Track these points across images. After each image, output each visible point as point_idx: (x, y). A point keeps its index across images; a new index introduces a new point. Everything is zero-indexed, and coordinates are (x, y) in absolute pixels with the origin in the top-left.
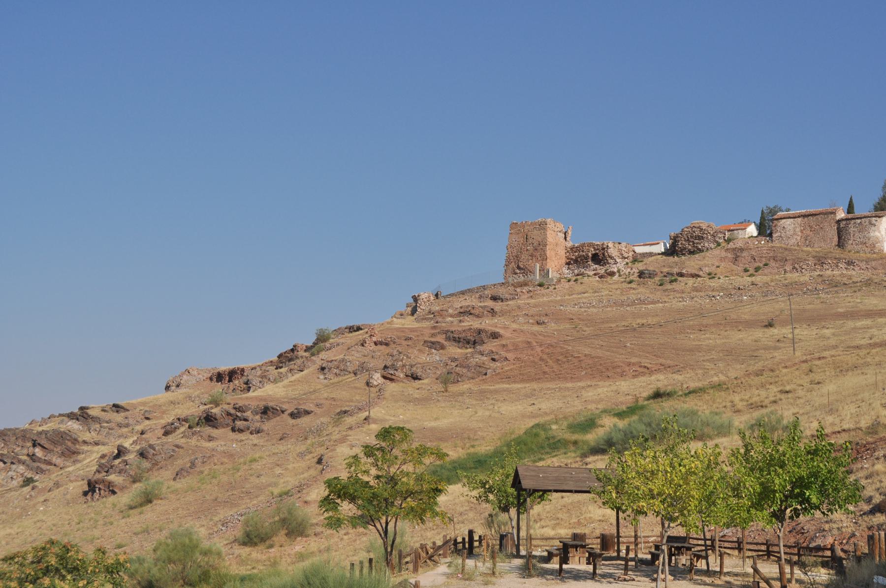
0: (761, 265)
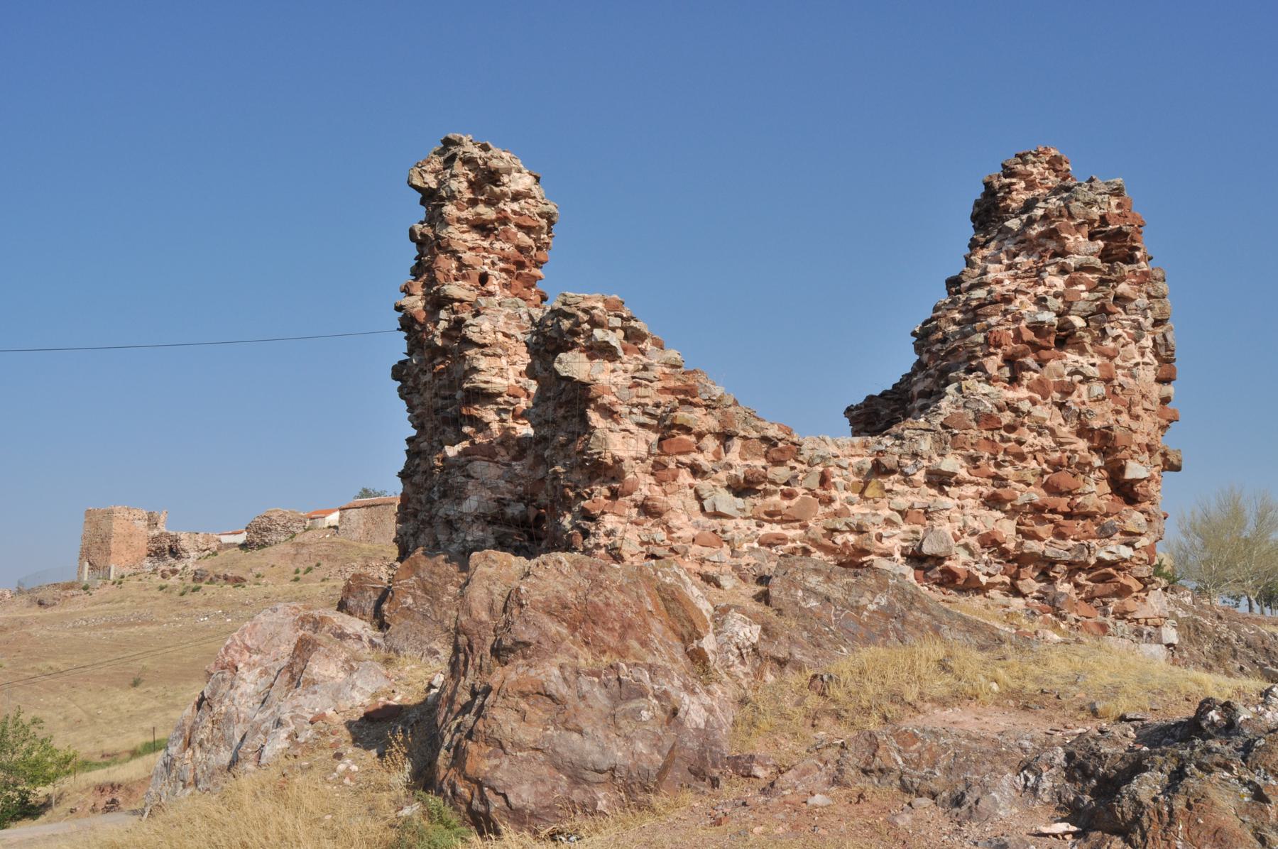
0: (313, 564)
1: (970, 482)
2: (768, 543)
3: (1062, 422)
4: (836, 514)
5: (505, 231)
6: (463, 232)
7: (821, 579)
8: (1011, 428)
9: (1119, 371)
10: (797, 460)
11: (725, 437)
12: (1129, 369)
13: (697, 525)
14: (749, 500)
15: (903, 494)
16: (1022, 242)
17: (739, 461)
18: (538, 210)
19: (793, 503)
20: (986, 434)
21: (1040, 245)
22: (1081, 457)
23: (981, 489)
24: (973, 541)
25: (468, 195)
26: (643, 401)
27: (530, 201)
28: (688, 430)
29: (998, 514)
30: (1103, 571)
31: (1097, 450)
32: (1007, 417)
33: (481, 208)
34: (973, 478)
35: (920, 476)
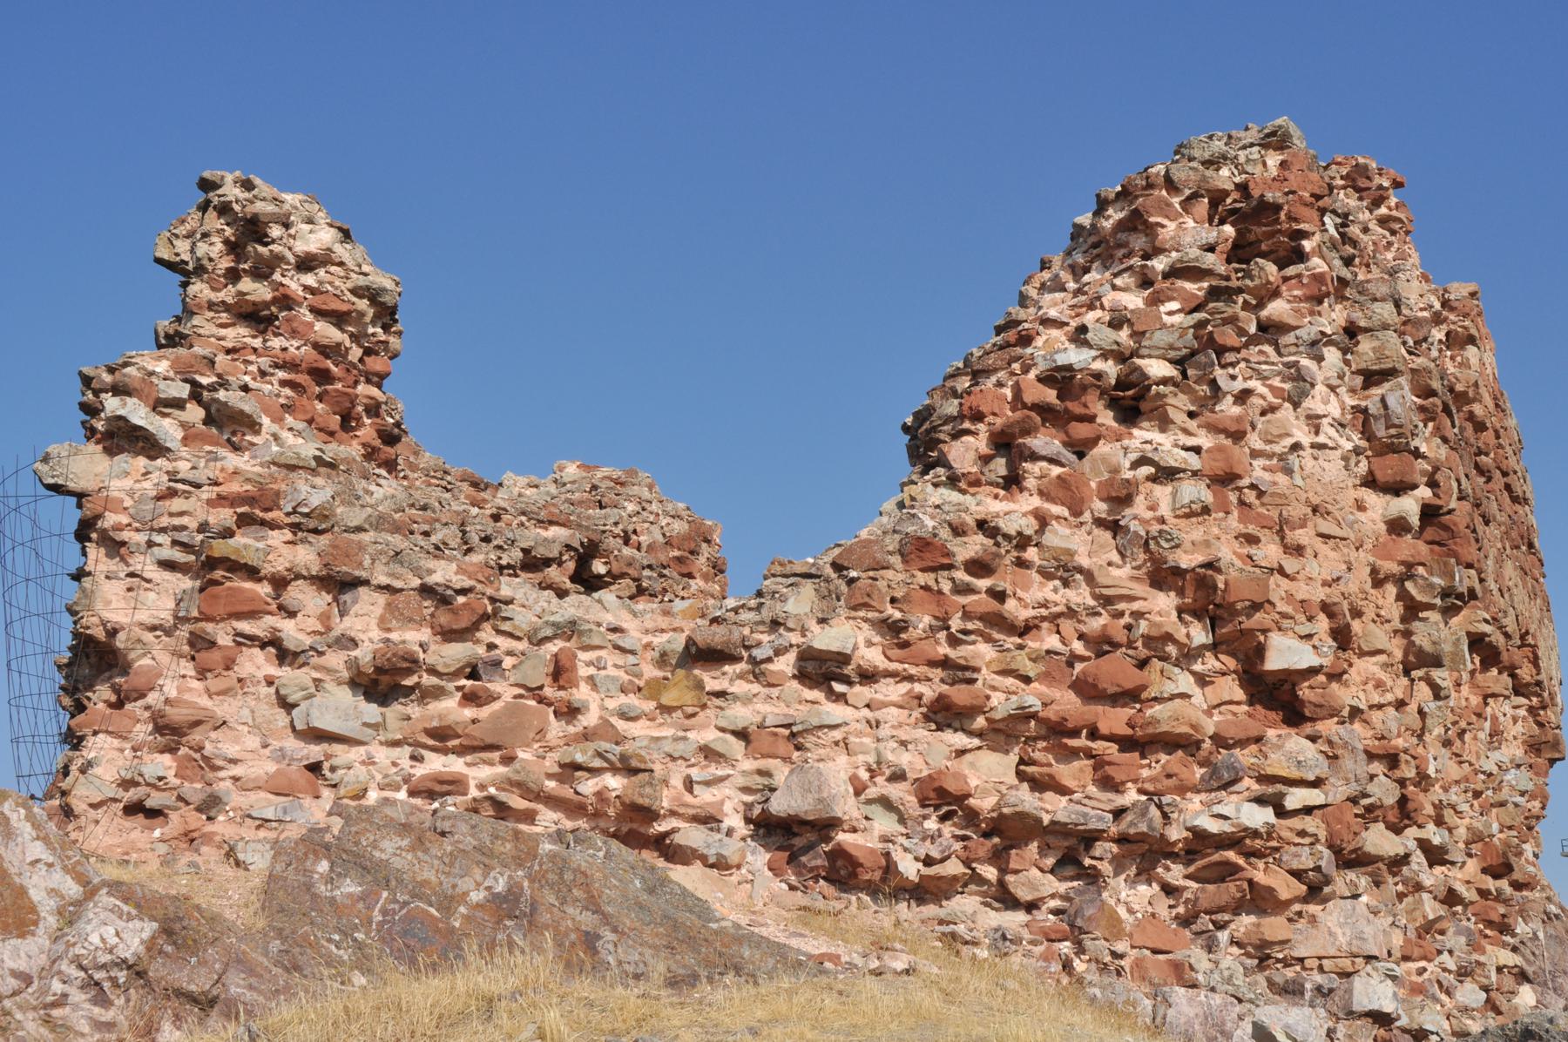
2: (431, 790)
3: (1116, 558)
4: (586, 736)
5: (288, 320)
7: (405, 843)
8: (979, 567)
9: (1258, 463)
10: (499, 632)
11: (339, 585)
12: (1282, 457)
13: (281, 755)
14: (396, 709)
15: (747, 700)
16: (1095, 246)
17: (367, 625)
18: (350, 285)
19: (484, 712)
20: (923, 578)
21: (1120, 246)
22: (1152, 624)
23: (918, 688)
24: (897, 792)
25: (226, 263)
26: (177, 521)
27: (333, 269)
28: (252, 573)
29: (960, 740)
30: (1216, 857)
31: (1198, 614)
32: (975, 545)
33: (246, 284)
35: (785, 665)
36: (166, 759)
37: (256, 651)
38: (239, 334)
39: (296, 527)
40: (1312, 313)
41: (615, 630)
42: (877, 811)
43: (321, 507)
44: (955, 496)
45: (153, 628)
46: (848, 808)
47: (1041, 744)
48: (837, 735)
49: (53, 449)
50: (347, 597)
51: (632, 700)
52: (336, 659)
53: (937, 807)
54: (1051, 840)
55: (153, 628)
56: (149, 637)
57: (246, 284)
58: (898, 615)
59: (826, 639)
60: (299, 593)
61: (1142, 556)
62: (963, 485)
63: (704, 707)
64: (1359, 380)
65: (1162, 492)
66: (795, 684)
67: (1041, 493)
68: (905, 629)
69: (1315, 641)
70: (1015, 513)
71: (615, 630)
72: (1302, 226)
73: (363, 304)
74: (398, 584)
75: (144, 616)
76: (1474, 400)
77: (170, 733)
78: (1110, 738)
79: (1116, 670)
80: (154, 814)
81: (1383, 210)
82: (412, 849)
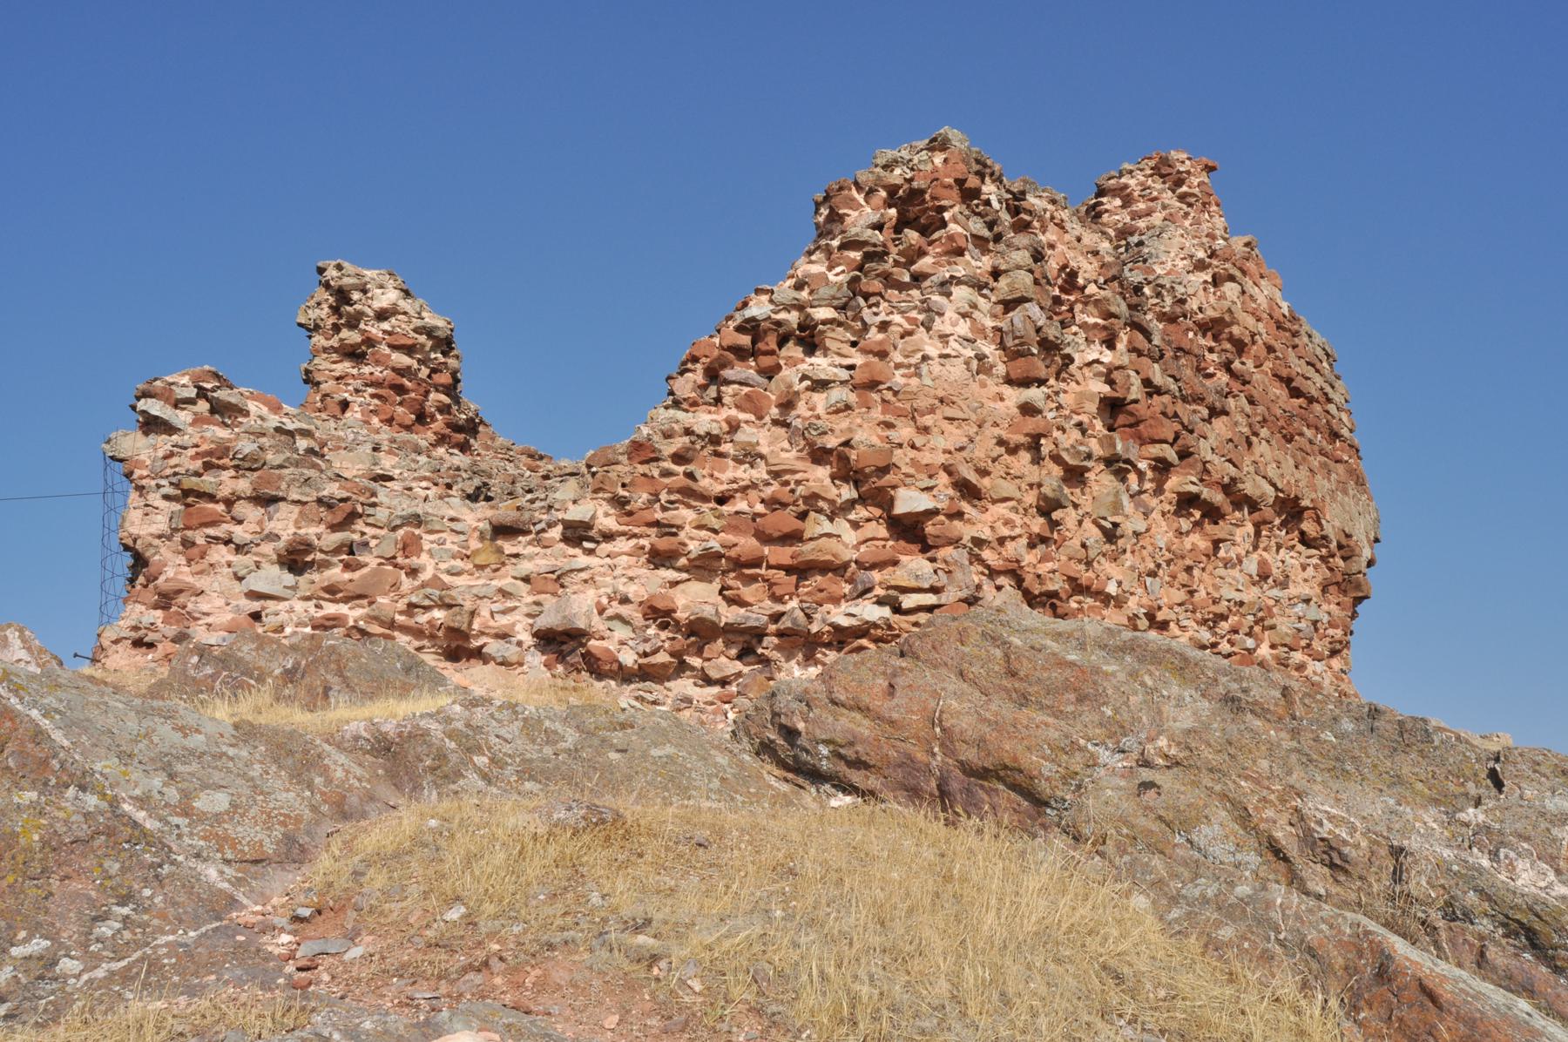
1: (623, 534)
3: (786, 445)
6: (334, 362)
8: (679, 458)
12: (917, 366)
13: (238, 609)
15: (531, 558)
17: (285, 524)
19: (357, 575)
20: (642, 469)
23: (643, 542)
24: (625, 610)
28: (211, 498)
31: (845, 479)
32: (680, 442)
33: (345, 333)
34: (625, 528)
35: (556, 533)
36: (159, 613)
37: (221, 547)
38: (346, 366)
39: (237, 468)
40: (949, 263)
41: (452, 520)
42: (616, 624)
43: (251, 453)
44: (680, 415)
45: (160, 537)
46: (598, 624)
47: (732, 575)
48: (584, 575)
49: (113, 435)
50: (271, 509)
51: (458, 563)
52: (267, 548)
53: (655, 620)
54: (731, 636)
55: (160, 537)
56: (156, 542)
57: (345, 333)
58: (626, 494)
59: (576, 513)
60: (242, 508)
61: (803, 443)
62: (685, 406)
63: (503, 564)
64: (1000, 308)
65: (820, 400)
66: (562, 545)
67: (737, 406)
68: (628, 502)
69: (935, 492)
70: (705, 420)
71: (452, 520)
72: (943, 203)
73: (422, 339)
74: (304, 499)
75: (154, 529)
76: (1229, 325)
77: (165, 600)
78: (779, 567)
79: (785, 520)
80: (151, 645)
81: (1184, 189)
82: (257, 649)
